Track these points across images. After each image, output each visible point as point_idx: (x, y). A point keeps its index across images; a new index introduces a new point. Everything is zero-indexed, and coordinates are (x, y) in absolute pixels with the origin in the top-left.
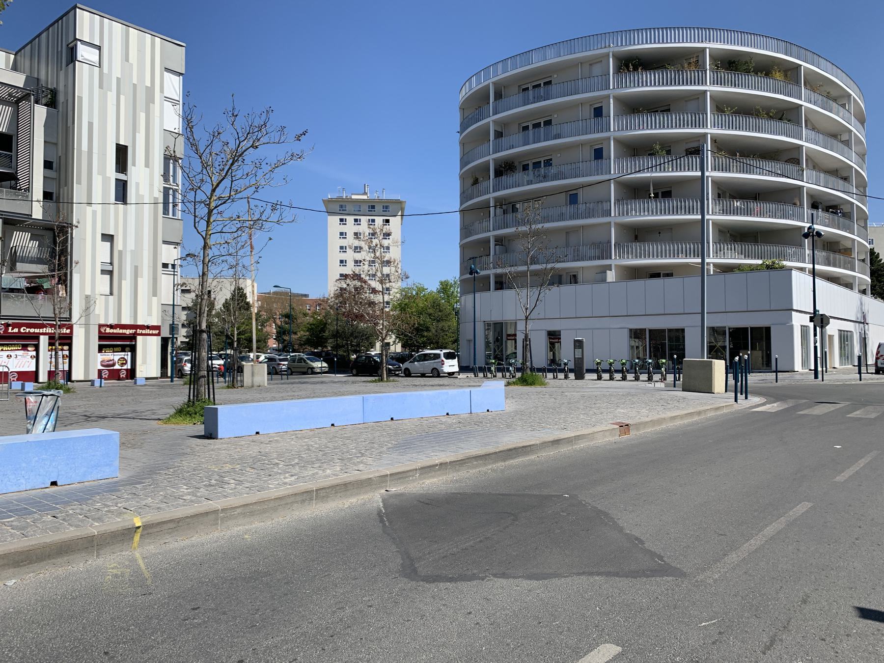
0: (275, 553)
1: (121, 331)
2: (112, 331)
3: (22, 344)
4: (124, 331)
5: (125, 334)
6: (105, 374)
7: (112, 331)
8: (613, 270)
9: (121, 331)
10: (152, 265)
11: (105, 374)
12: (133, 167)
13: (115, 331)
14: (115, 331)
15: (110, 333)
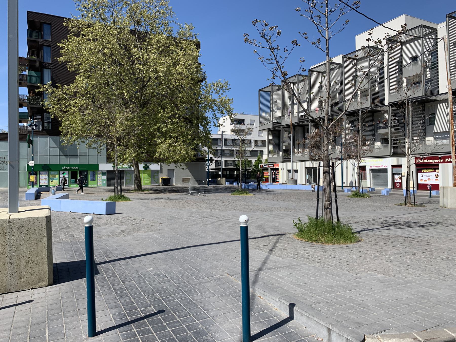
0: (132, 12)
1: (429, 161)
2: (422, 161)
3: (434, 168)
4: (431, 161)
5: (432, 163)
6: (398, 185)
7: (422, 161)
8: (251, 159)
9: (429, 161)
10: (335, 172)
11: (398, 185)
12: (345, 192)
13: (425, 161)
14: (425, 161)
15: (421, 163)
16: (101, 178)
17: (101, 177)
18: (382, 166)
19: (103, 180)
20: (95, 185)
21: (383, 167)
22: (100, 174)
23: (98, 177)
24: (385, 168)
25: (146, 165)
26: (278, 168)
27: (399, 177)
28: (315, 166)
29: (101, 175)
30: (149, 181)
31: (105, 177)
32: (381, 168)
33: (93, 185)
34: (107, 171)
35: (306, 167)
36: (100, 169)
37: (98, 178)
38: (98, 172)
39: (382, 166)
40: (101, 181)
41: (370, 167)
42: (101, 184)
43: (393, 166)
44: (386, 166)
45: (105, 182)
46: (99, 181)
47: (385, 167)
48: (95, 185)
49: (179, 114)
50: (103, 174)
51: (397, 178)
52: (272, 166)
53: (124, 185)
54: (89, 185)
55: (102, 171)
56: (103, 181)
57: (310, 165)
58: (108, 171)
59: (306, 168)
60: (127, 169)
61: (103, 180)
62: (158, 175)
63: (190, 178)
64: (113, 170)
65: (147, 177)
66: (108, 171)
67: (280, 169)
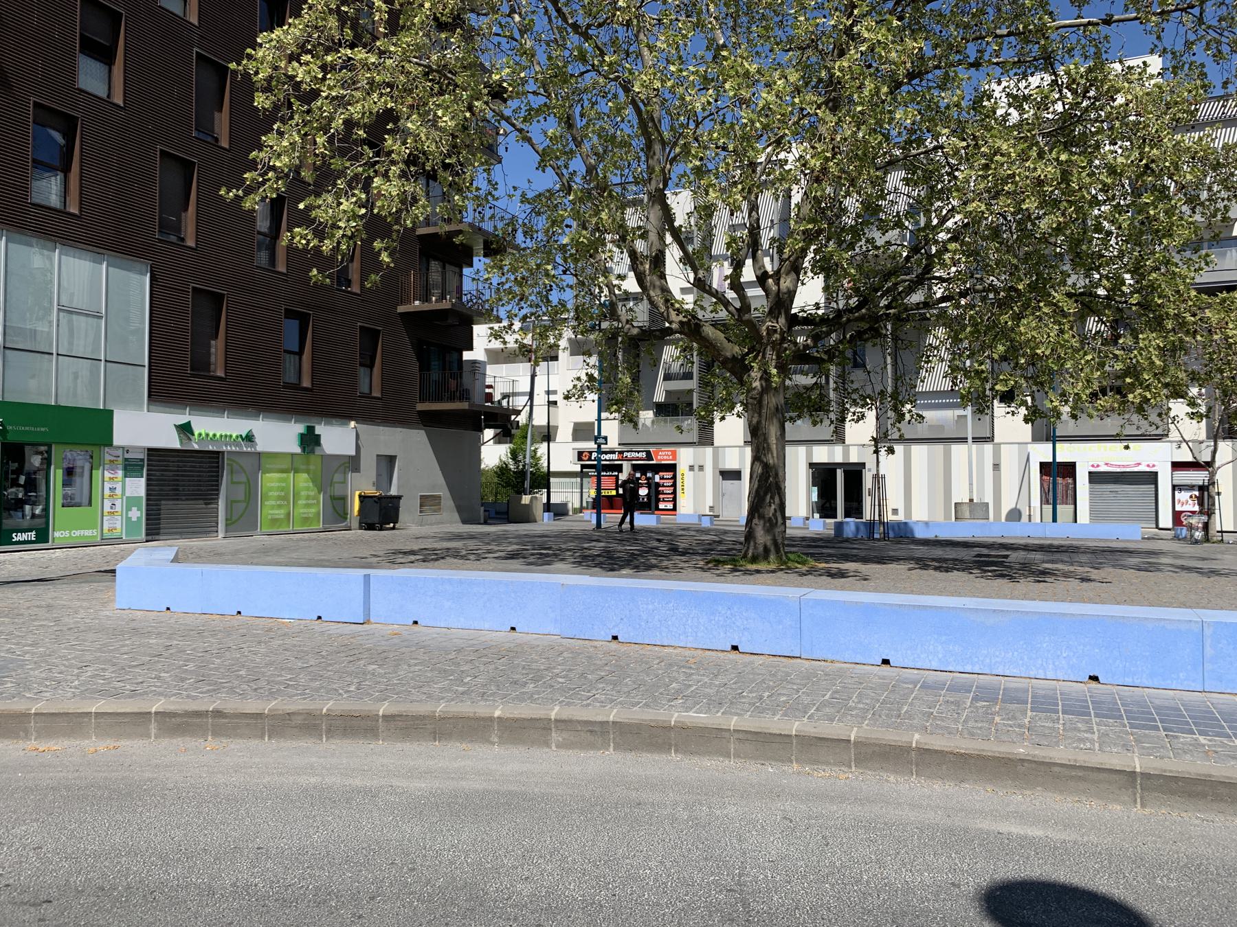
16: (119, 491)
17: (119, 487)
18: (1139, 464)
19: (131, 502)
20: (88, 533)
21: (1143, 468)
22: (113, 466)
23: (107, 486)
24: (1148, 469)
25: (311, 429)
26: (675, 465)
27: (1191, 497)
28: (854, 459)
29: (120, 473)
30: (313, 510)
31: (138, 487)
32: (1136, 469)
33: (78, 533)
34: (150, 450)
35: (815, 460)
36: (118, 440)
37: (107, 492)
38: (108, 458)
39: (1139, 464)
40: (118, 508)
41: (1093, 466)
42: (118, 526)
43: (1177, 466)
44: (1154, 466)
45: (138, 514)
46: (107, 509)
47: (1148, 466)
48: (88, 533)
49: (885, 221)
50: (131, 468)
51: (1183, 499)
52: (644, 455)
53: (221, 526)
54: (57, 534)
55: (126, 450)
56: (129, 509)
57: (831, 454)
58: (155, 454)
59: (811, 465)
60: (238, 445)
61: (131, 502)
62: (344, 482)
63: (439, 497)
64: (176, 445)
65: (308, 489)
66: (153, 452)
67: (682, 468)
